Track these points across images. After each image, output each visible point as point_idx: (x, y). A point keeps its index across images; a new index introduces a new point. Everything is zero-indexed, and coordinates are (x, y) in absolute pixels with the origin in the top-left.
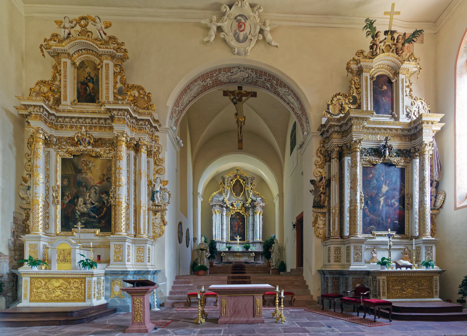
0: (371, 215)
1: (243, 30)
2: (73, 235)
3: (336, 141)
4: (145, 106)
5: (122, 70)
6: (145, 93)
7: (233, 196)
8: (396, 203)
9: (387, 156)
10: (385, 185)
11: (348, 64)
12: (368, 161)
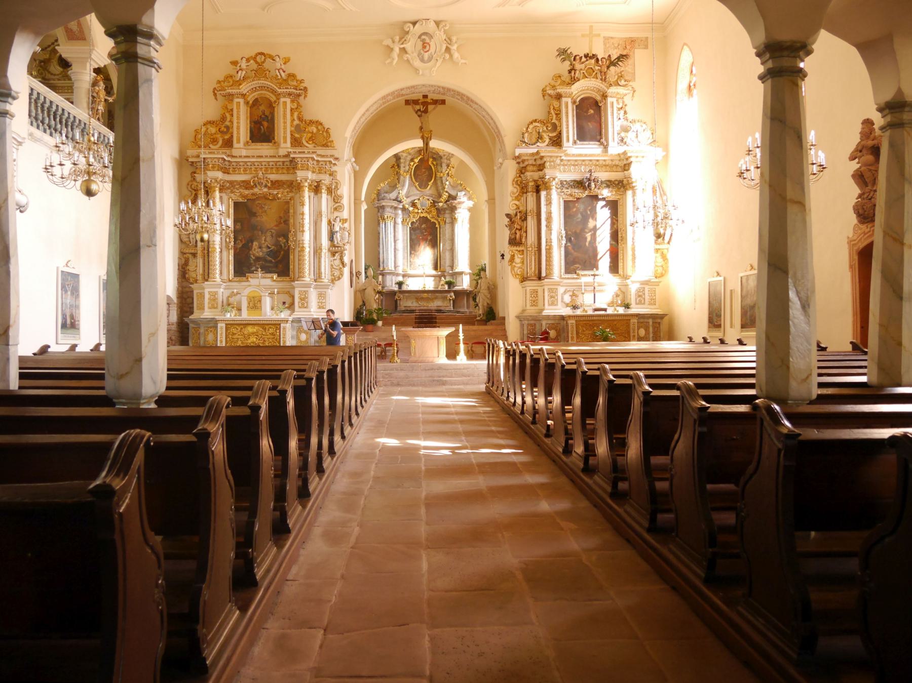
0: (575, 253)
1: (428, 51)
2: (248, 281)
3: (531, 175)
4: (324, 143)
5: (299, 105)
6: (324, 128)
7: (414, 188)
9: (593, 189)
11: (544, 90)
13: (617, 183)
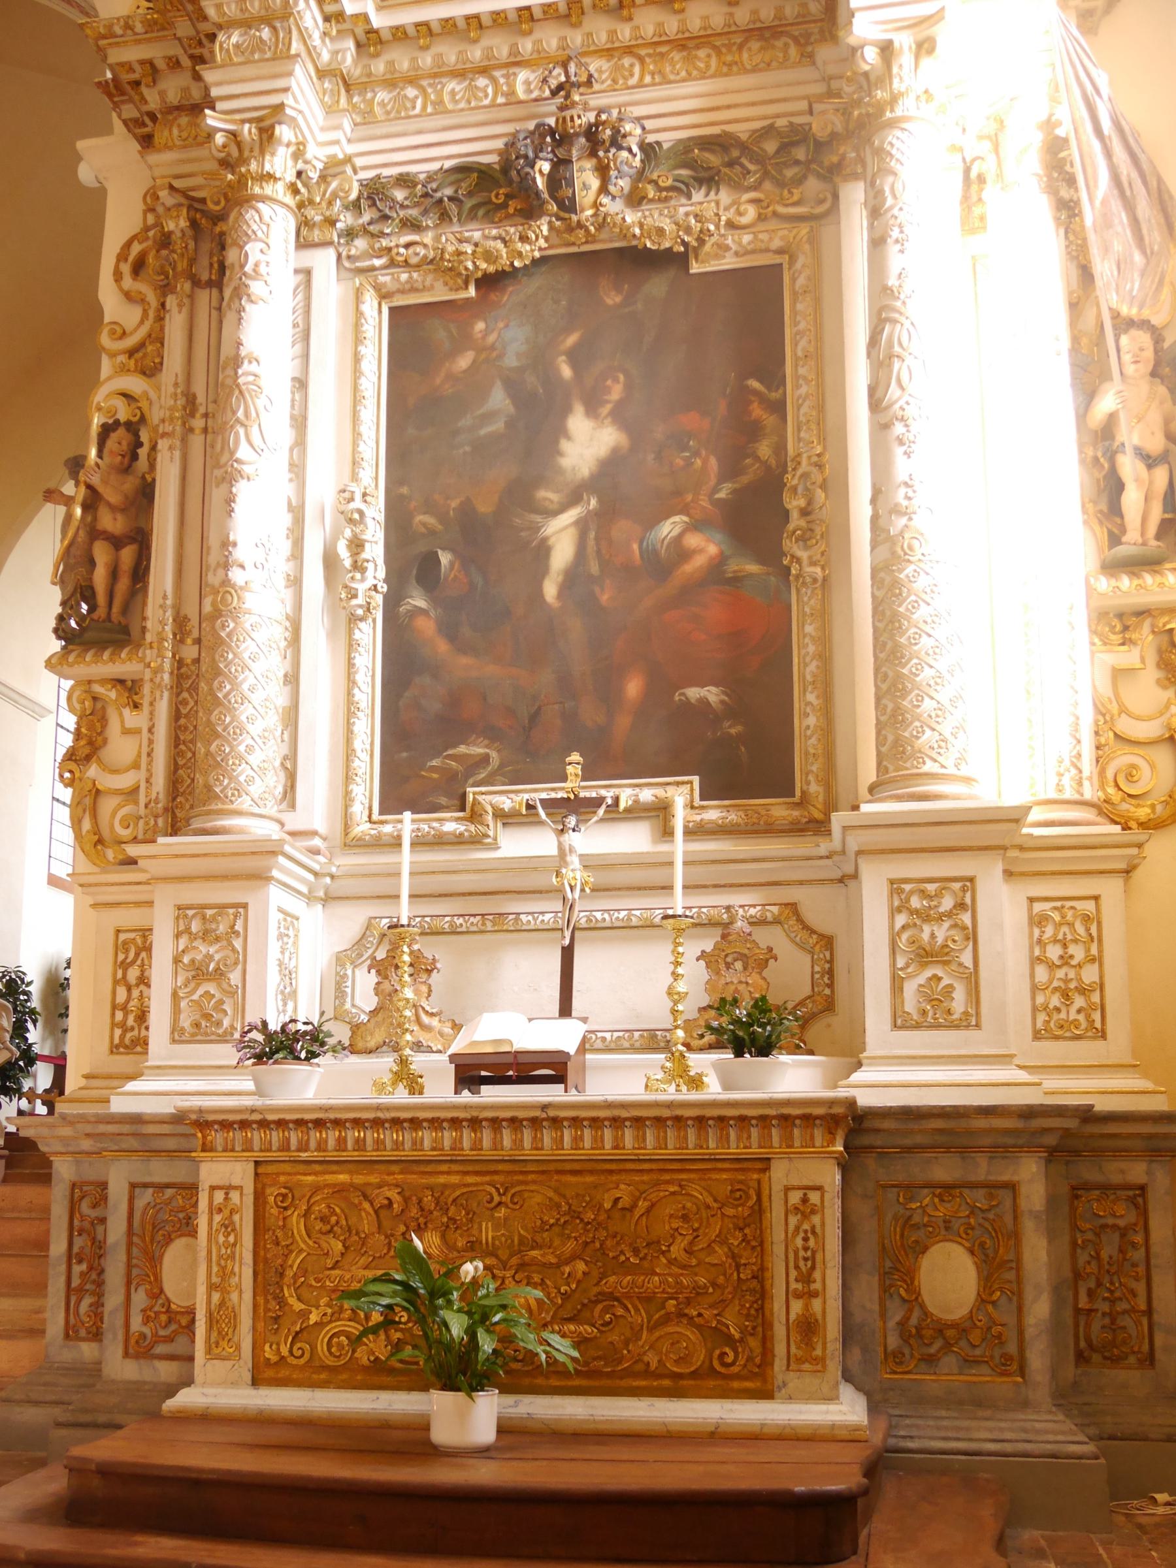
0: (464, 660)
8: (693, 540)
10: (592, 410)
12: (426, 262)
13: (771, 147)
